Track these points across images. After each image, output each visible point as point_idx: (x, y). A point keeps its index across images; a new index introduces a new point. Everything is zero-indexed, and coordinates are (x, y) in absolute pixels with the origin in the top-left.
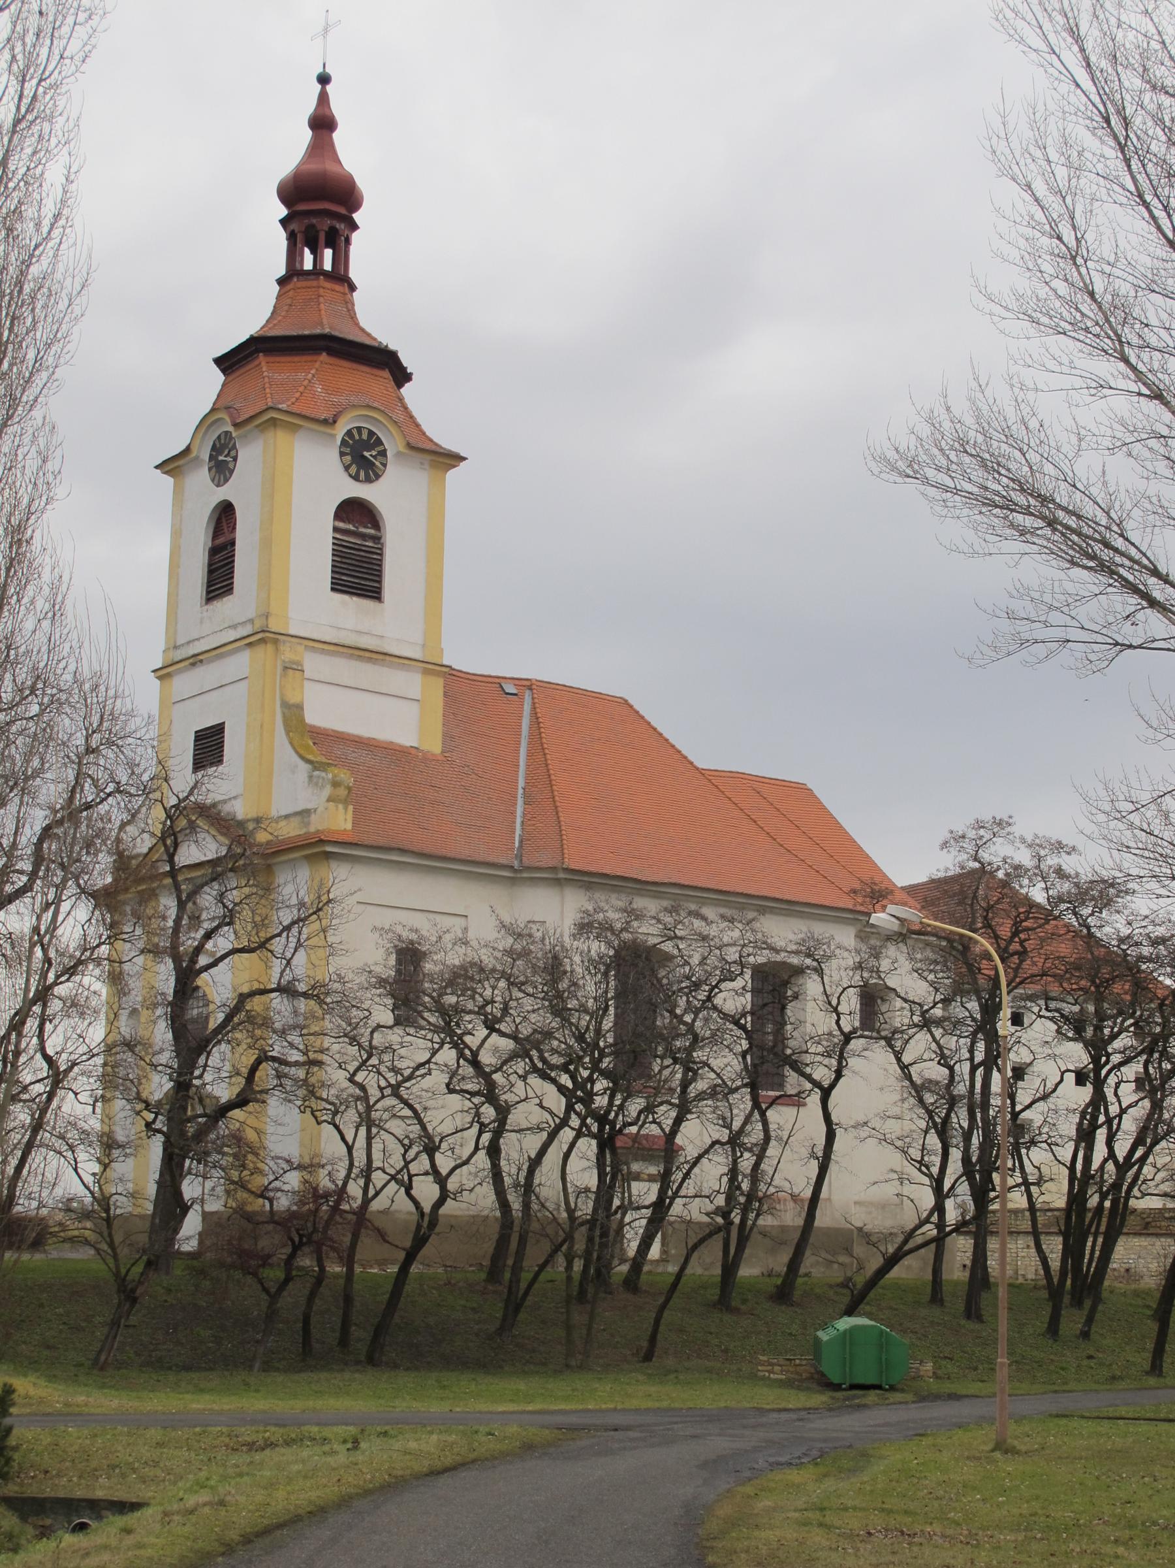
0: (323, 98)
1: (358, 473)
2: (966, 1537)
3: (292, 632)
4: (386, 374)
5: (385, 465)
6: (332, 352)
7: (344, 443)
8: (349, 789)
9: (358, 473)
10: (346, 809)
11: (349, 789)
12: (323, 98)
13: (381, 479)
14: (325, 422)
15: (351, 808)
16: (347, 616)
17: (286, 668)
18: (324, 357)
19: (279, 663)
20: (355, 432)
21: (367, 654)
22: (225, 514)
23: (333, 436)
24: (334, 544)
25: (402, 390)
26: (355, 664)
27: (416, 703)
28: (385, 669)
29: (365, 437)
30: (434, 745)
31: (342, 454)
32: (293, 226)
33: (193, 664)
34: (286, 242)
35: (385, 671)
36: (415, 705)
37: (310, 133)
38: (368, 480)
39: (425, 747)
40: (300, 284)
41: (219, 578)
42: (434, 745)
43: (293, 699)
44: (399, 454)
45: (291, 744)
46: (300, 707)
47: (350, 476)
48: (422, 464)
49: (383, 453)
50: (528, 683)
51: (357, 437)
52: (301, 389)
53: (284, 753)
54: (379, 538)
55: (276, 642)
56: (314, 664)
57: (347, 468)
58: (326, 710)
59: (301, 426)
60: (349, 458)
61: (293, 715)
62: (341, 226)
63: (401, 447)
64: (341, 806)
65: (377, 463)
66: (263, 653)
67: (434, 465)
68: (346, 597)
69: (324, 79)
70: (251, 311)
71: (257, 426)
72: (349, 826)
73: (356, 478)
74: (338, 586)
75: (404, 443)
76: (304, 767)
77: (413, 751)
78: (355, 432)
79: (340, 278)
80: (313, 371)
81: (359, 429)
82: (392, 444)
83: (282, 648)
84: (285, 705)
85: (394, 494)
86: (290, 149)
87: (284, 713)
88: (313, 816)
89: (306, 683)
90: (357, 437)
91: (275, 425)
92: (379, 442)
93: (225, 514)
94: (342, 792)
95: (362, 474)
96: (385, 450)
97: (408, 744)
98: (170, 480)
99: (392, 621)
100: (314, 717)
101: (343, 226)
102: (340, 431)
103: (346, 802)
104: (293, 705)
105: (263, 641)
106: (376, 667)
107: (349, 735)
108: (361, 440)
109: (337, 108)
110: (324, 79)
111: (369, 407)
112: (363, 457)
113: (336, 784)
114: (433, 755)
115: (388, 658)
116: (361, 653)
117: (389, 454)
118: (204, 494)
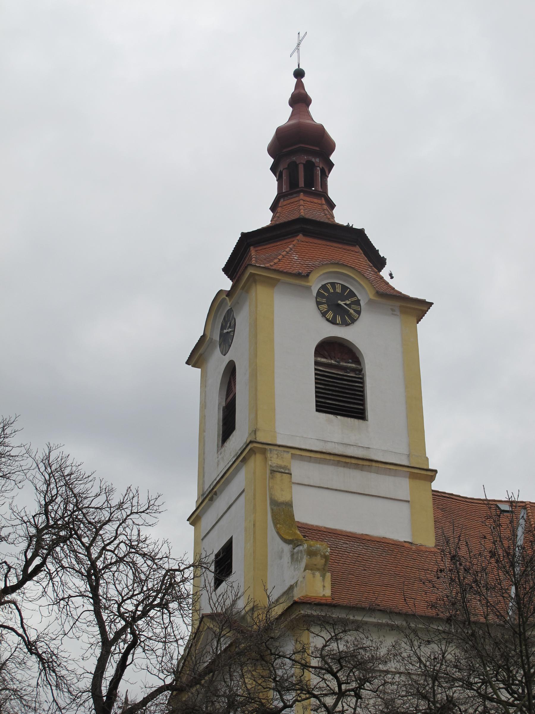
0: (299, 85)
1: (334, 317)
2: (77, 516)
3: (279, 443)
4: (357, 249)
5: (359, 313)
6: (306, 233)
7: (319, 294)
8: (326, 557)
9: (334, 317)
10: (323, 576)
11: (326, 557)
12: (299, 85)
13: (357, 323)
14: (299, 276)
15: (328, 575)
16: (335, 432)
17: (273, 472)
18: (300, 237)
19: (268, 468)
20: (329, 286)
21: (353, 461)
22: (231, 371)
23: (309, 288)
24: (316, 374)
25: (381, 273)
26: (341, 470)
27: (406, 505)
28: (373, 476)
29: (339, 290)
30: (428, 540)
31: (318, 303)
32: (281, 168)
33: (211, 499)
34: (277, 182)
35: (373, 476)
36: (405, 506)
37: (291, 109)
38: (345, 324)
39: (418, 541)
40: (285, 203)
41: (228, 426)
42: (428, 540)
43: (282, 497)
44: (370, 302)
45: (278, 533)
46: (289, 505)
47: (328, 320)
48: (393, 310)
49: (358, 302)
50: (523, 504)
51: (332, 291)
52: (280, 257)
53: (275, 544)
54: (361, 370)
55: (264, 452)
56: (300, 470)
57: (324, 314)
58: (313, 508)
59: (278, 280)
60: (325, 306)
61: (282, 513)
62: (316, 160)
63: (371, 295)
64: (318, 574)
65: (352, 311)
66: (256, 463)
67: (404, 311)
68: (331, 416)
69: (299, 74)
70: (263, 219)
71: (243, 288)
72: (328, 592)
73: (333, 322)
74: (322, 407)
75: (374, 292)
76: (287, 548)
77: (407, 545)
78: (329, 286)
79: (323, 195)
80: (291, 246)
81: (333, 284)
82: (364, 294)
83: (269, 455)
84: (274, 503)
85: (369, 334)
86: (283, 115)
87: (272, 510)
88: (295, 589)
89: (294, 487)
90: (332, 291)
91: (255, 281)
92: (352, 294)
93: (231, 371)
94: (319, 561)
95: (339, 319)
96: (358, 301)
97: (402, 540)
98: (197, 371)
99: (375, 434)
100: (304, 514)
101: (318, 160)
102: (316, 283)
103: (323, 571)
104: (282, 503)
105: (252, 452)
106: (364, 473)
107: (341, 531)
108: (335, 292)
109: (309, 90)
110: (299, 74)
111: (337, 264)
112: (338, 305)
113: (311, 553)
114: (429, 548)
115: (374, 464)
116: (348, 460)
117: (362, 303)
118: (217, 362)
